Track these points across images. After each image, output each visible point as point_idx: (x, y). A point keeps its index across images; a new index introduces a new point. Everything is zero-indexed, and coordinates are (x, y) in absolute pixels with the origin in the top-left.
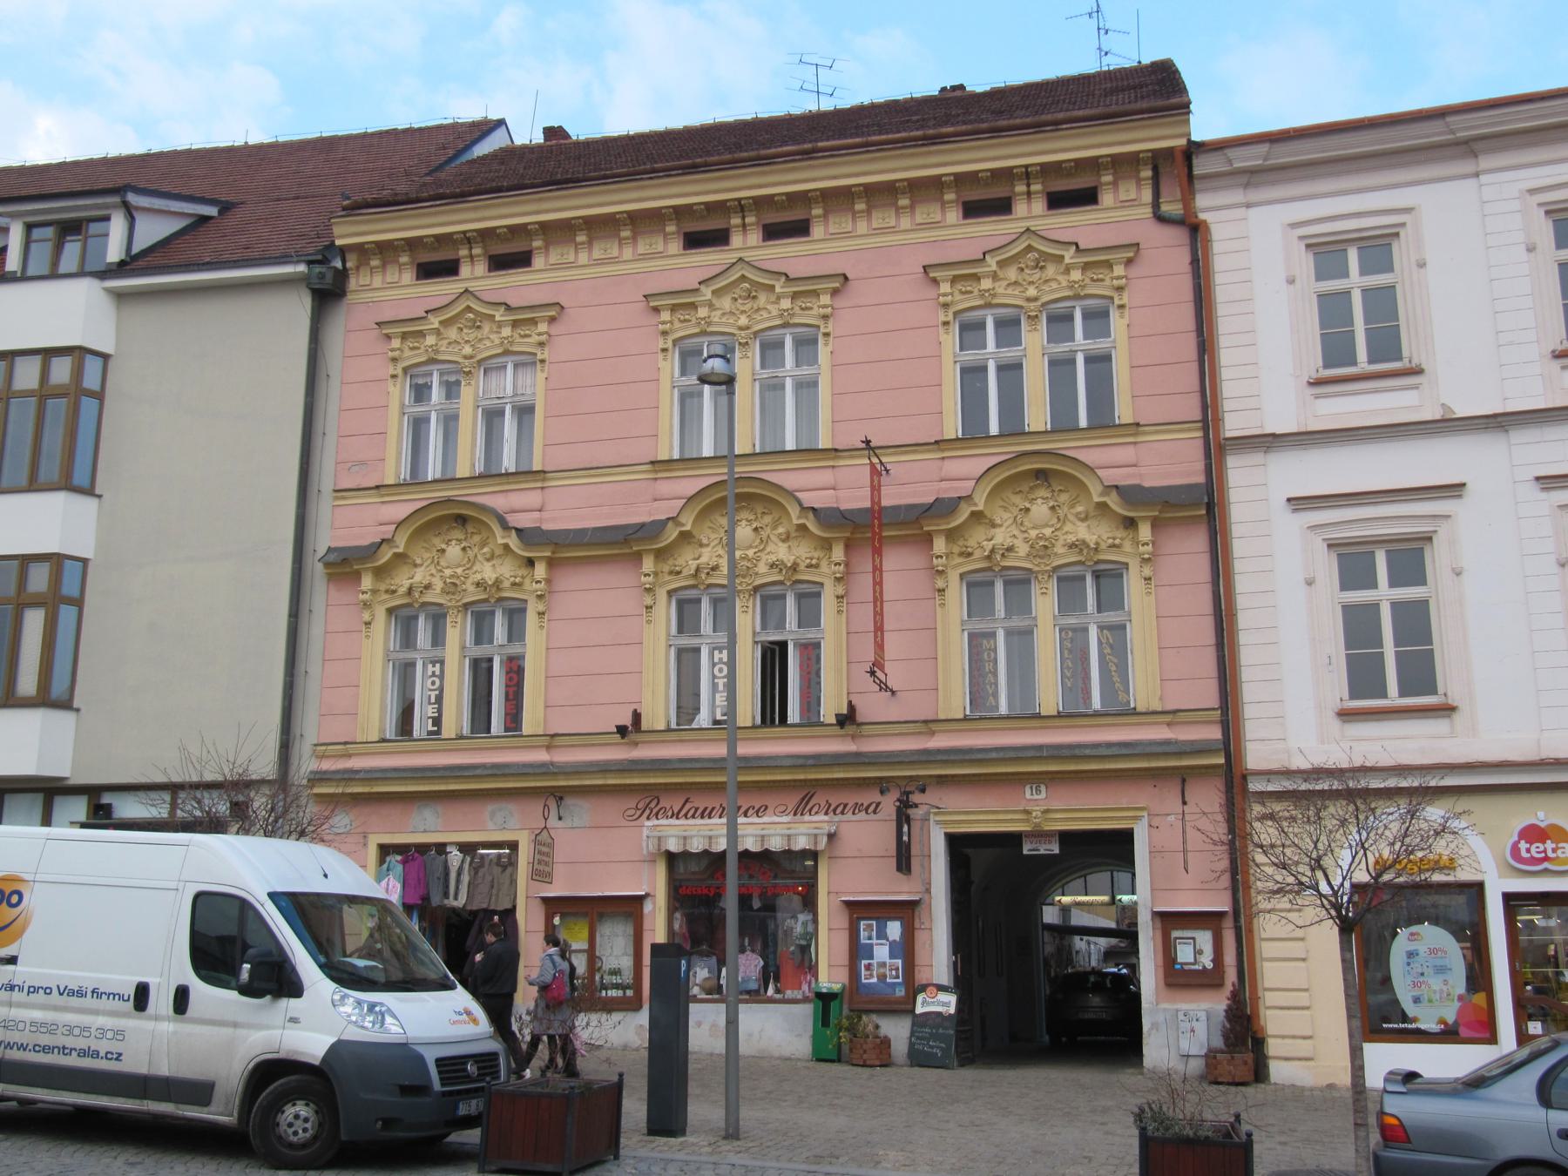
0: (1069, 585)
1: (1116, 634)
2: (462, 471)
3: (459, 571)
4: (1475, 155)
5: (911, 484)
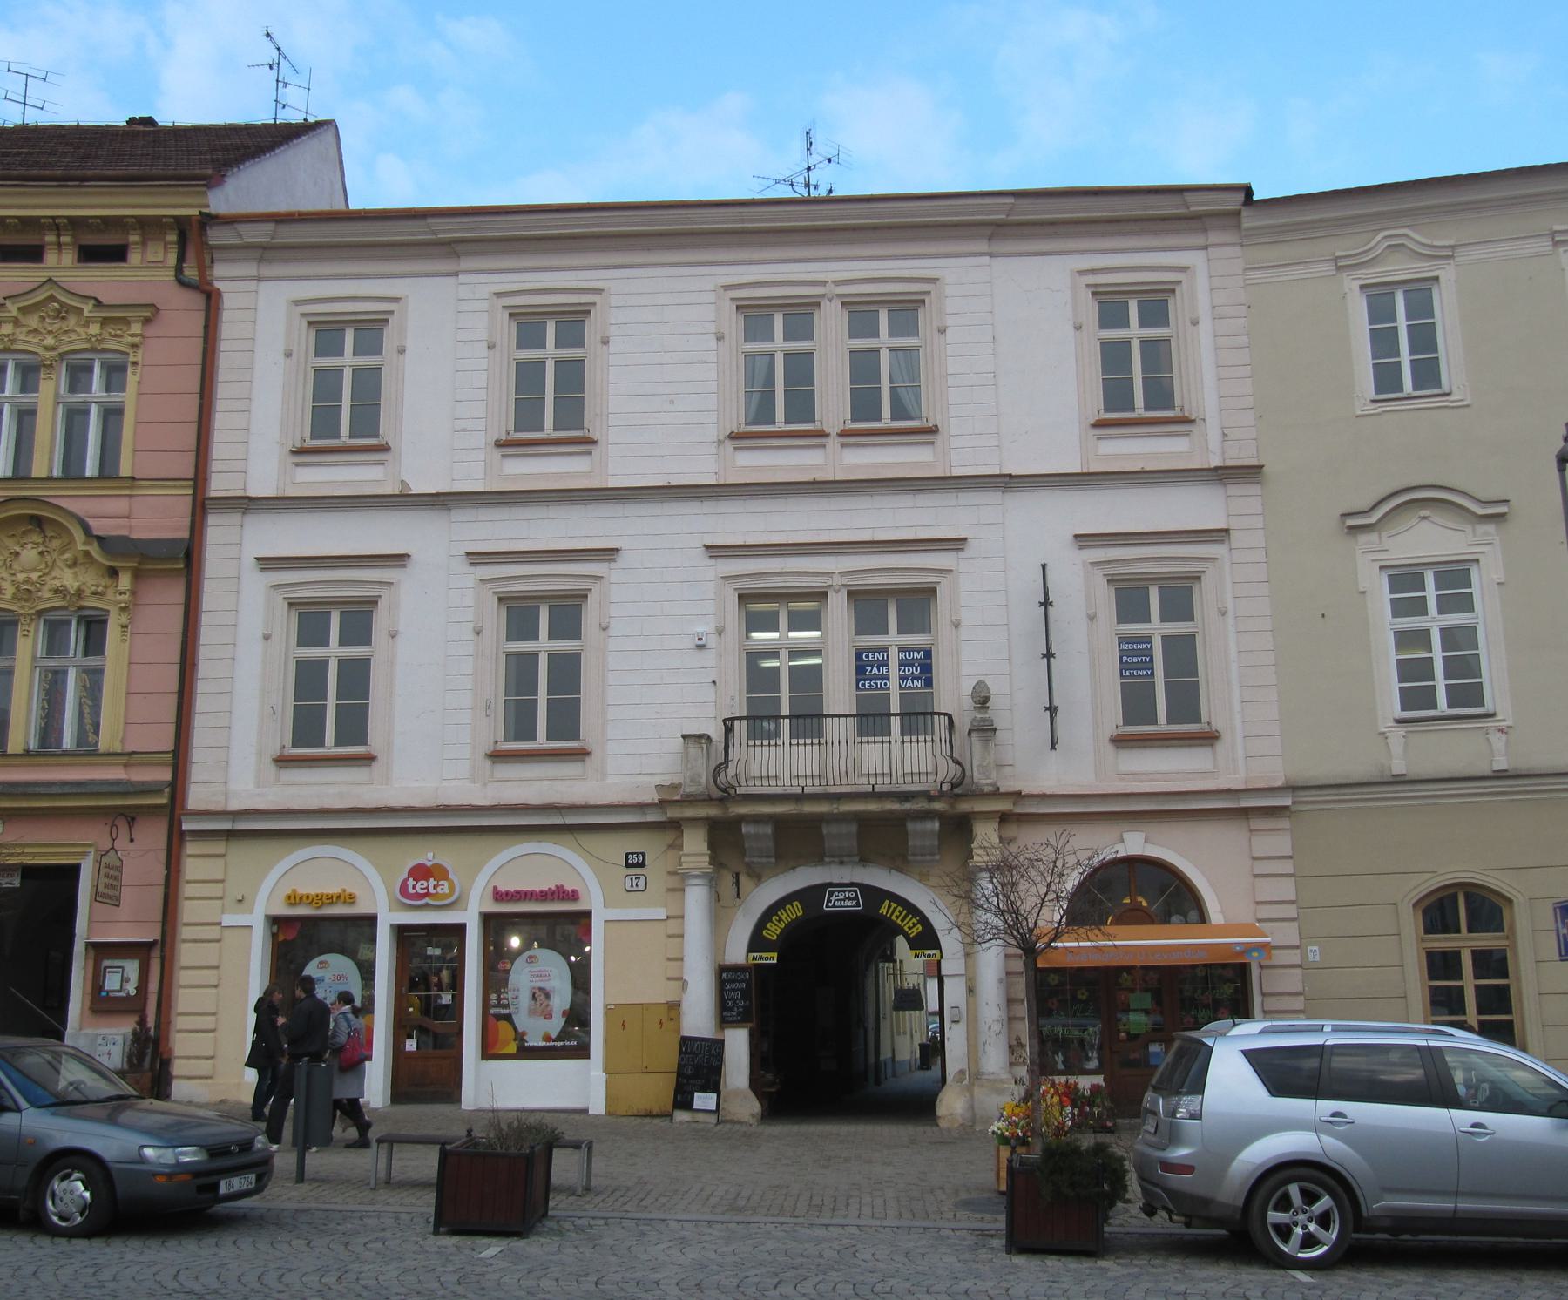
0: (55, 633)
2: (39, 470)
3: (35, 576)
4: (457, 255)
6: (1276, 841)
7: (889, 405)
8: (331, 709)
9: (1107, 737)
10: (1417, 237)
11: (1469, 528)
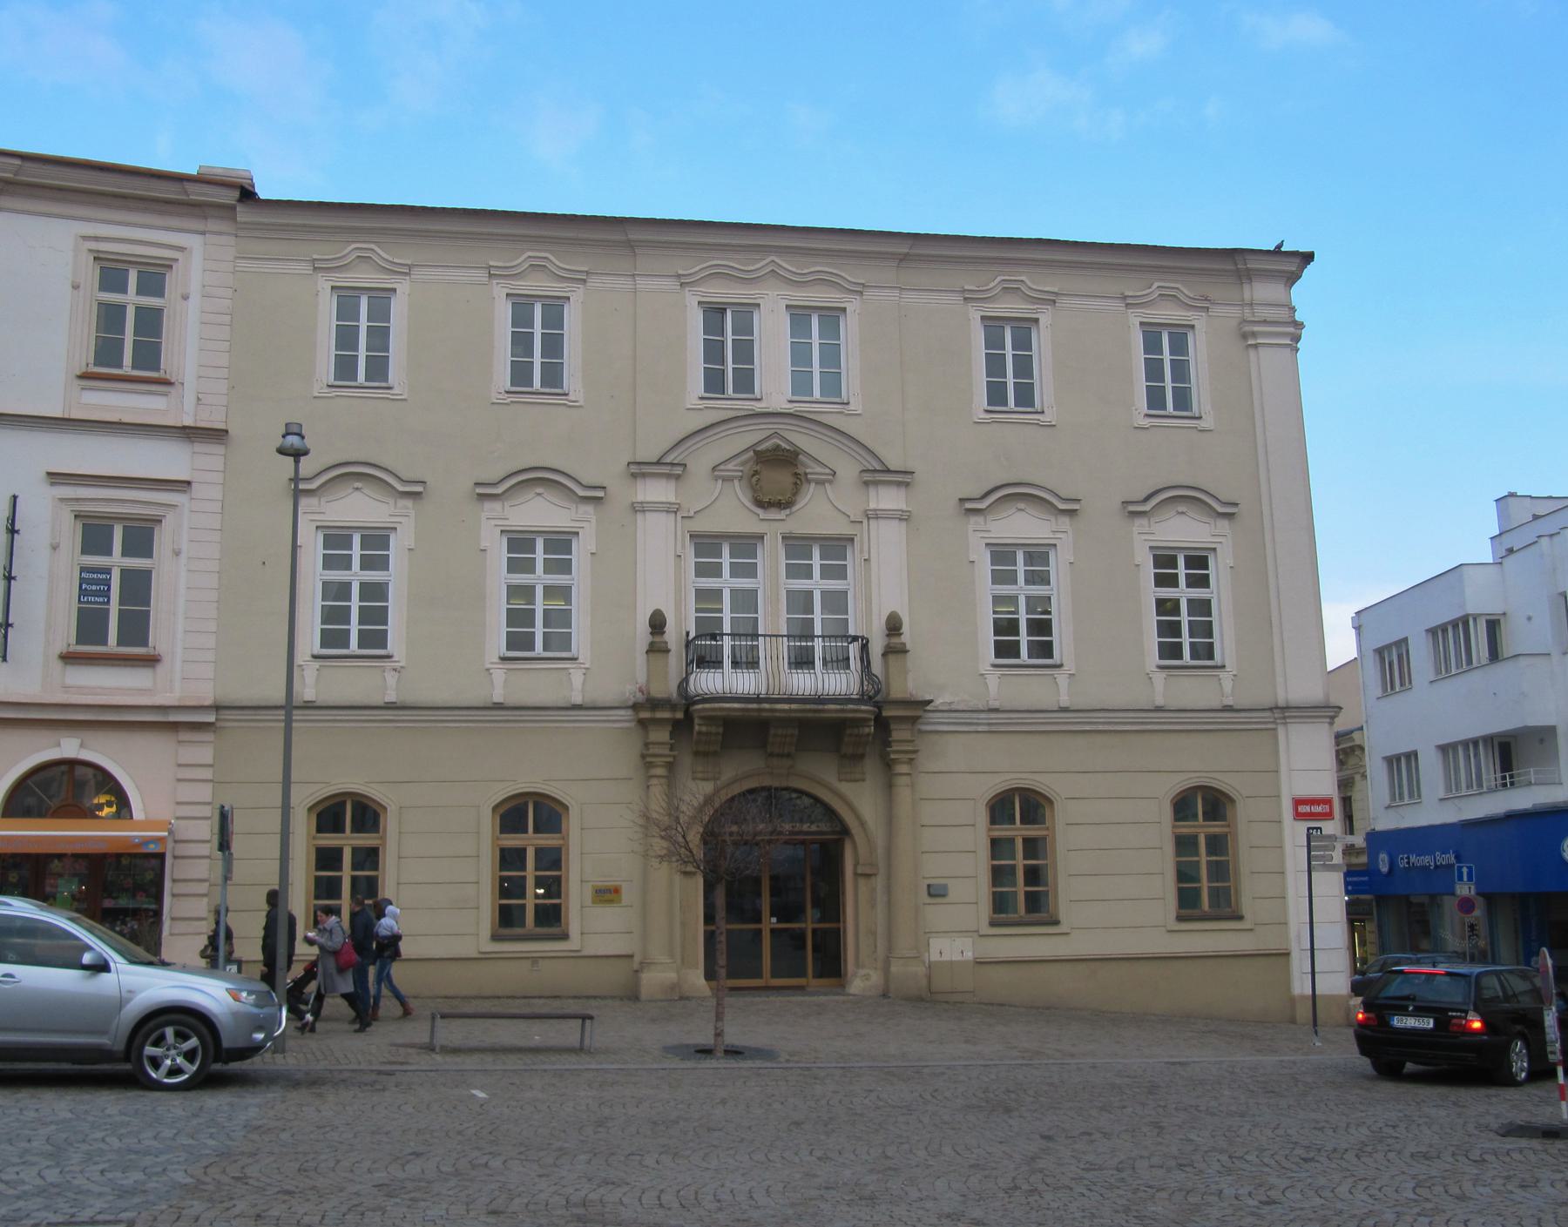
6: (201, 751)
9: (58, 652)
10: (556, 261)
11: (391, 501)
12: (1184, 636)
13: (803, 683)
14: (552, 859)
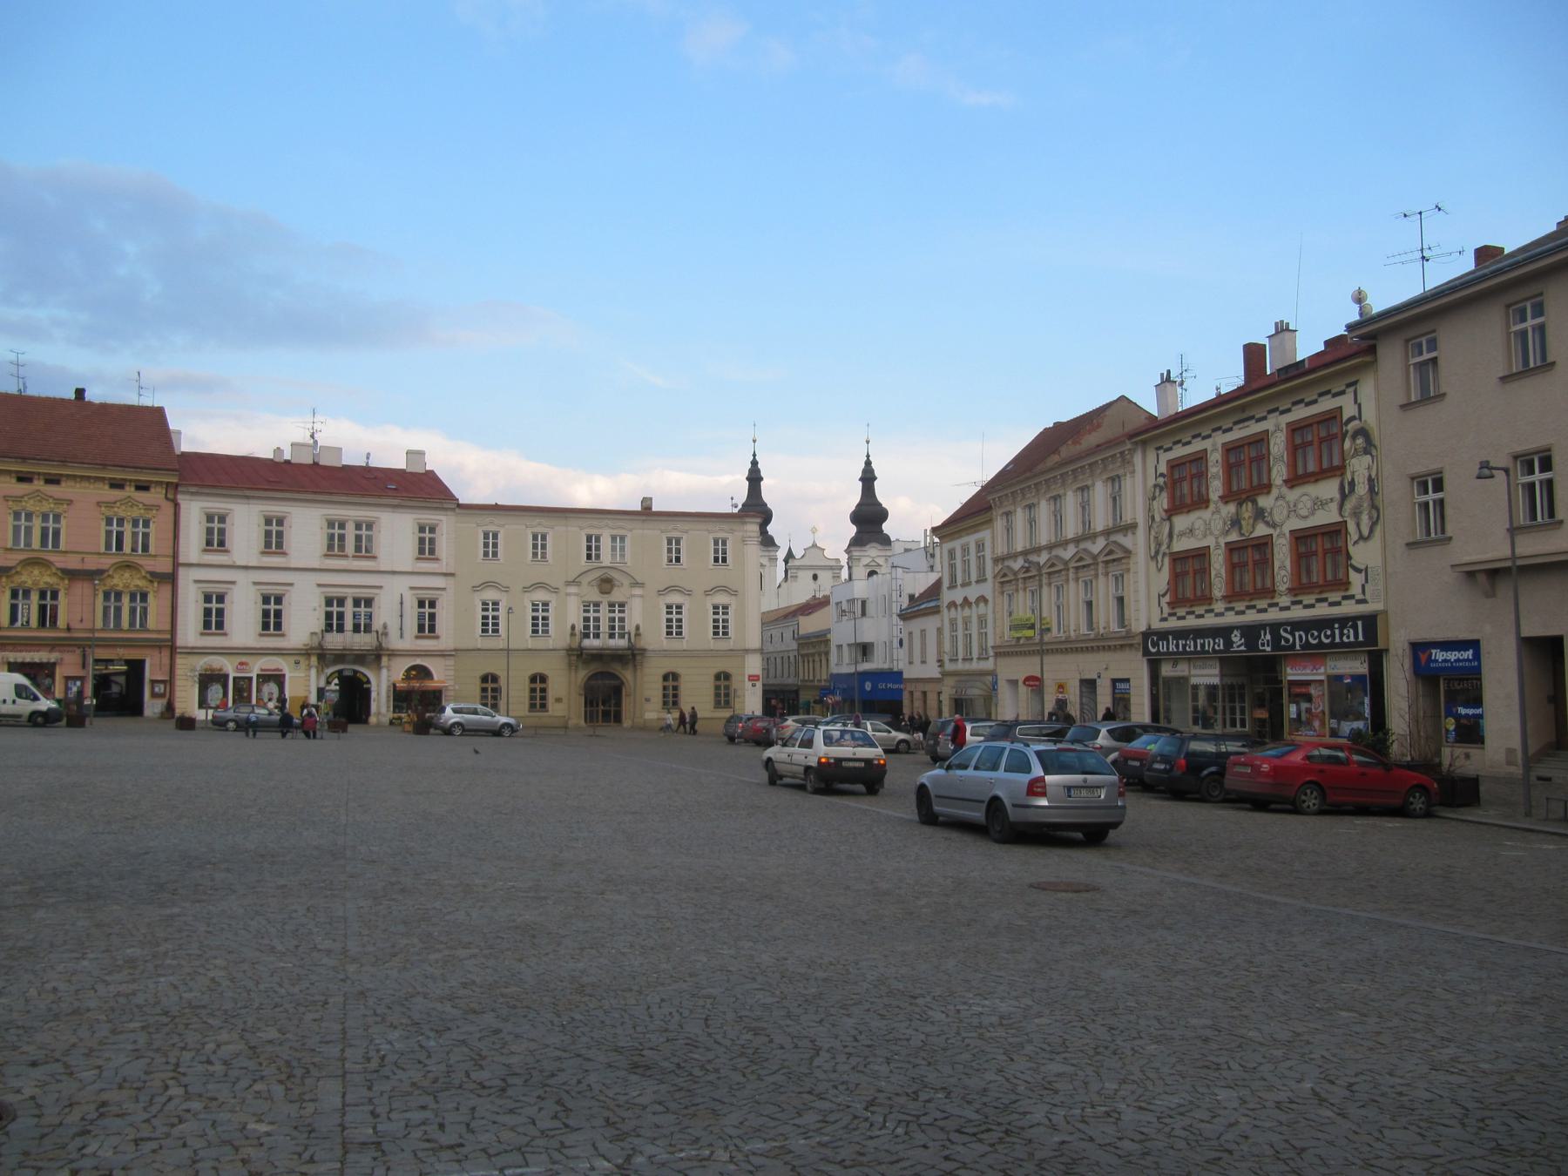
0: (133, 598)
1: (145, 610)
5: (92, 564)
6: (451, 662)
7: (364, 548)
8: (214, 620)
12: (720, 630)
13: (612, 643)
14: (543, 690)
